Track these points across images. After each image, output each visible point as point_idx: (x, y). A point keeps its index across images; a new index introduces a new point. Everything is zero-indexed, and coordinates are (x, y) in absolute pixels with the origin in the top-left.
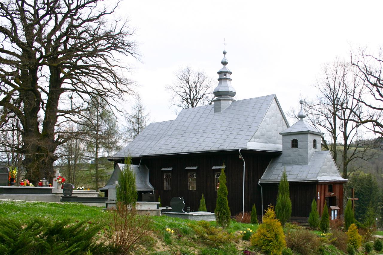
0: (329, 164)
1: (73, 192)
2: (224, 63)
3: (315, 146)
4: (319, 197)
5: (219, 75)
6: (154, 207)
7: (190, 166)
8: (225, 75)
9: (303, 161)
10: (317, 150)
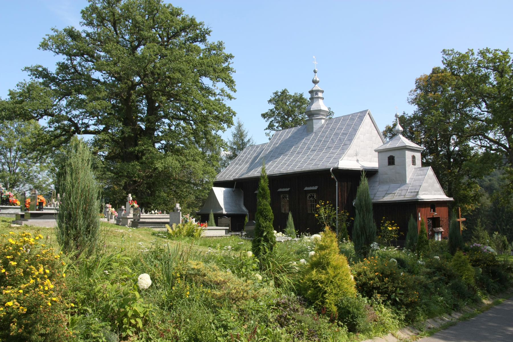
0: (430, 181)
1: (141, 217)
3: (414, 163)
4: (420, 219)
6: (223, 233)
7: (282, 188)
8: (317, 94)
9: (401, 180)
10: (416, 167)
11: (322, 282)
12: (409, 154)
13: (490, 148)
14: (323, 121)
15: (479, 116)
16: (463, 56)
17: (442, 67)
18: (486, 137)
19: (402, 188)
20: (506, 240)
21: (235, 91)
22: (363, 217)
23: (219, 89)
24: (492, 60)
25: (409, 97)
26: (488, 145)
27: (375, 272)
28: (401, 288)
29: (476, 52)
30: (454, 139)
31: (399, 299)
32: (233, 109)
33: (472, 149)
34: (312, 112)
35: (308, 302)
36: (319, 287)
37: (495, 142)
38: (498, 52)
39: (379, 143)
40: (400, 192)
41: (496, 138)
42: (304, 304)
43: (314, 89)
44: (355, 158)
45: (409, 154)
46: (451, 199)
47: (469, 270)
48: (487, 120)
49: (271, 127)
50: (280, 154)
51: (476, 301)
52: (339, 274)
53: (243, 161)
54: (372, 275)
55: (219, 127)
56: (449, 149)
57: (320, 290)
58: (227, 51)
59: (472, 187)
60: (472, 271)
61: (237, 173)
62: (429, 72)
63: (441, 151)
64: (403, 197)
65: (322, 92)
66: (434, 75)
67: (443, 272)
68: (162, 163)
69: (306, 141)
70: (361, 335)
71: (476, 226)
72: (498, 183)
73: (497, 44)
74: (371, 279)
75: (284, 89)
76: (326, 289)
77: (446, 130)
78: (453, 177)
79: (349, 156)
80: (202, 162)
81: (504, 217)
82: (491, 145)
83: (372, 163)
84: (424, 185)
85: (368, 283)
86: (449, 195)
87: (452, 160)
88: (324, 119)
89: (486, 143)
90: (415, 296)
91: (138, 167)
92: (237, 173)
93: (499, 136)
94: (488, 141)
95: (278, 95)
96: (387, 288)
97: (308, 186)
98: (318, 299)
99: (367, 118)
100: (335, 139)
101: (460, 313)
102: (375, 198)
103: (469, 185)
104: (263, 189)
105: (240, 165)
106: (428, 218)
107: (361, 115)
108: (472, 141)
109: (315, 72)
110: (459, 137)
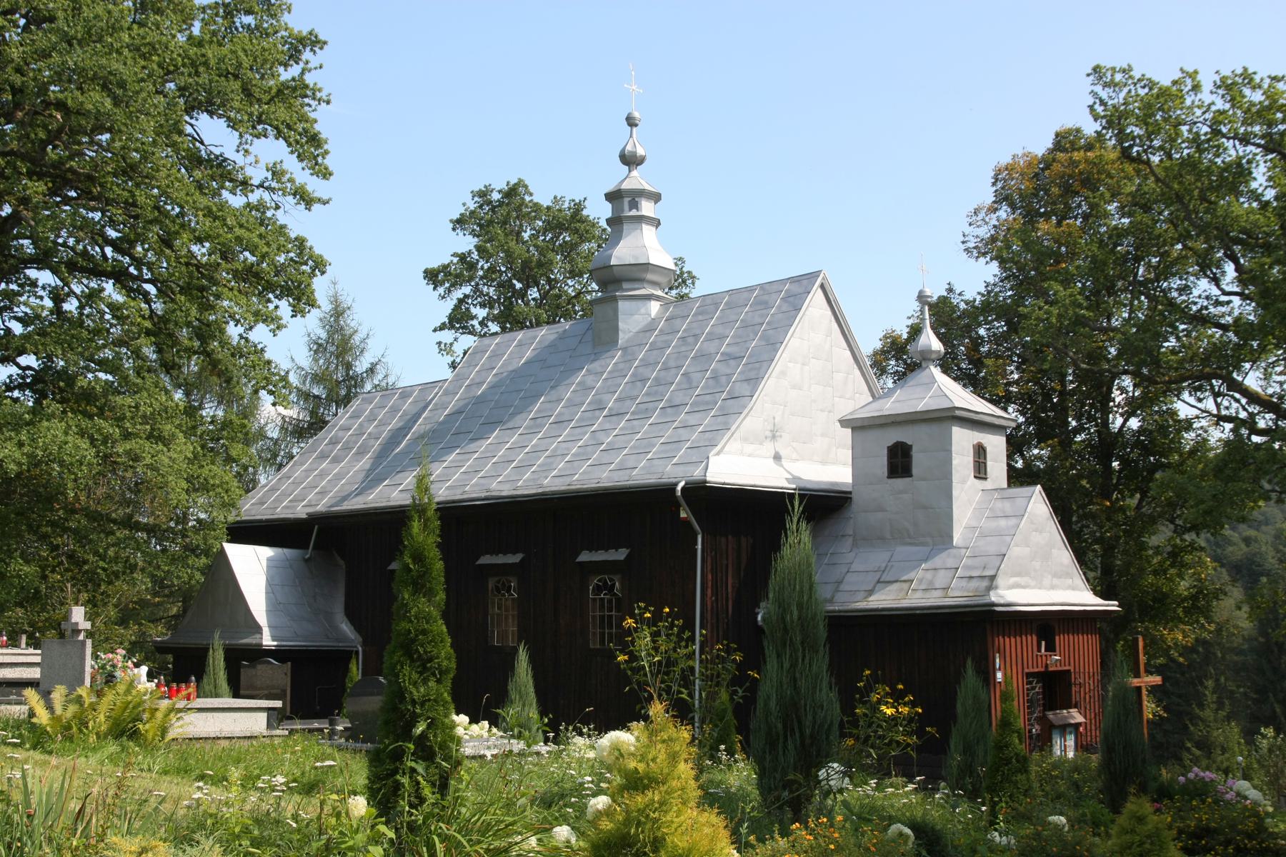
3: (980, 471)
4: (999, 675)
5: (610, 206)
8: (634, 205)
9: (933, 530)
12: (963, 439)
14: (655, 307)
15: (1212, 309)
17: (1091, 128)
19: (937, 561)
21: (326, 174)
22: (793, 666)
23: (262, 165)
25: (968, 230)
26: (1243, 415)
30: (1124, 388)
32: (318, 245)
33: (1188, 425)
40: (929, 575)
41: (1270, 391)
43: (625, 186)
44: (769, 449)
45: (963, 439)
46: (1113, 606)
50: (492, 424)
53: (347, 448)
56: (1106, 423)
58: (297, 21)
59: (1184, 565)
61: (323, 493)
62: (1041, 145)
64: (938, 593)
65: (656, 197)
68: (21, 445)
69: (590, 380)
75: (513, 181)
79: (745, 440)
82: (1252, 415)
83: (832, 467)
84: (1016, 552)
86: (1104, 591)
88: (658, 298)
89: (1235, 406)
92: (323, 493)
94: (1244, 401)
99: (815, 304)
100: (696, 376)
102: (840, 597)
103: (1175, 555)
104: (419, 558)
105: (336, 460)
106: (1029, 675)
107: (796, 288)
108: (1186, 395)
109: (631, 122)
110: (1140, 381)
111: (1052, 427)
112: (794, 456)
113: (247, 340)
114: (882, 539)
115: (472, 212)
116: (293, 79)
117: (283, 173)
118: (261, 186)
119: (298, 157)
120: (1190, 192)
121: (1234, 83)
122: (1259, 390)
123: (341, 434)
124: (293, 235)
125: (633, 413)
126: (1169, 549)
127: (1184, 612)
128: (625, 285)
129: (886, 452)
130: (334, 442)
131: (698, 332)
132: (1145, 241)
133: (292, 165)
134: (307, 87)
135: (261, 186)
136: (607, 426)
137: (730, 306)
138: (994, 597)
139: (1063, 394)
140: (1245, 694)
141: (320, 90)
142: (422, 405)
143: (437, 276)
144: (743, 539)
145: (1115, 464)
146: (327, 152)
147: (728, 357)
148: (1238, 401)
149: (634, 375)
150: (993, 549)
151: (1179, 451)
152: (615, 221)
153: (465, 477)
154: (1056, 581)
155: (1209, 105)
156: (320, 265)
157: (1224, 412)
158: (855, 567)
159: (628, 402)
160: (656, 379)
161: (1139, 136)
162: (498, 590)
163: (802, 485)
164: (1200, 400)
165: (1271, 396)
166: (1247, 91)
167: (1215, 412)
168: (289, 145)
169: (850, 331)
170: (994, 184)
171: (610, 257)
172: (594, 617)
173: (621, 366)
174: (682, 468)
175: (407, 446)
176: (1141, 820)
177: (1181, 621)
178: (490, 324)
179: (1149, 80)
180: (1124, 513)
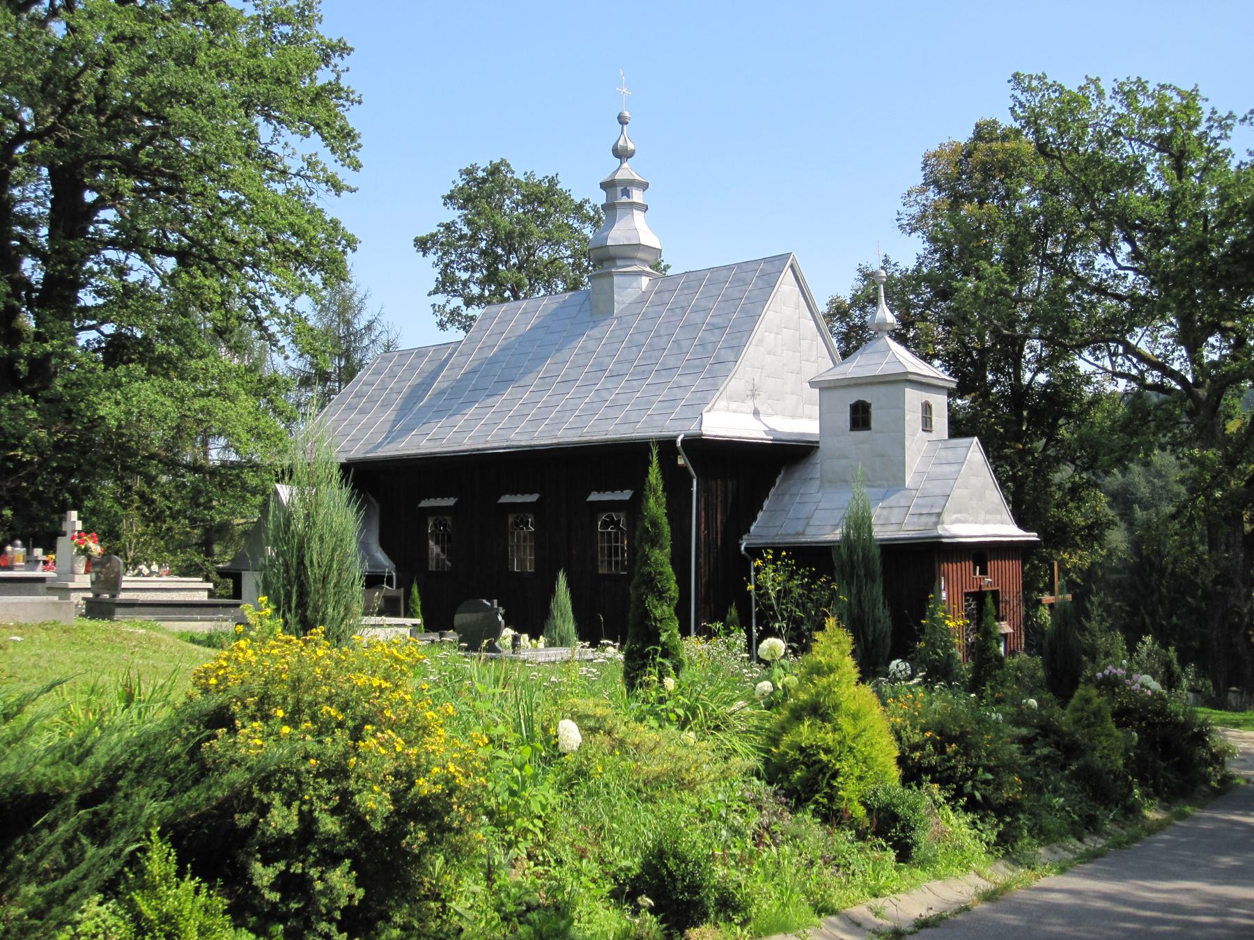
1: (124, 585)
2: (621, 154)
3: (927, 425)
4: (944, 594)
7: (514, 492)
8: (626, 193)
9: (890, 475)
11: (828, 751)
12: (913, 398)
13: (1139, 380)
14: (645, 282)
15: (1110, 282)
16: (1074, 99)
17: (1007, 122)
18: (1130, 350)
19: (892, 501)
20: (1175, 661)
21: (357, 167)
22: (859, 592)
23: (298, 156)
24: (1154, 117)
25: (902, 209)
26: (1134, 372)
27: (924, 731)
28: (988, 769)
29: (1107, 86)
30: (1033, 348)
31: (983, 796)
32: (349, 226)
33: (1087, 380)
34: (612, 252)
35: (797, 798)
36: (820, 761)
37: (1154, 365)
38: (1168, 93)
39: (818, 357)
40: (885, 513)
41: (1157, 352)
42: (786, 804)
43: (618, 176)
44: (749, 406)
45: (913, 398)
46: (1033, 537)
47: (1109, 735)
48: (1132, 297)
49: (446, 283)
50: (506, 381)
51: (1132, 811)
52: (864, 730)
53: (372, 401)
54: (917, 738)
55: (301, 287)
56: (1018, 378)
57: (824, 768)
58: (327, 31)
59: (1081, 499)
60: (1117, 738)
61: (354, 440)
62: (964, 136)
63: (993, 384)
64: (894, 527)
65: (644, 186)
66: (981, 145)
67: (1053, 737)
68: (117, 403)
69: (591, 345)
70: (918, 872)
71: (1088, 618)
72: (1149, 482)
73: (1166, 67)
74: (915, 747)
75: (497, 161)
76: (838, 766)
77: (1012, 322)
78: (1028, 465)
79: (731, 399)
80: (246, 403)
81: (1164, 590)
82: (1141, 372)
83: (801, 422)
84: (957, 493)
85: (908, 757)
86: (1021, 522)
87: (1025, 413)
88: (647, 274)
89: (1126, 365)
90: (1012, 790)
91: (32, 415)
92: (354, 440)
93: (1165, 346)
94: (1135, 360)
95: (475, 179)
96: (954, 768)
97: (600, 489)
98: (817, 792)
99: (786, 284)
100: (685, 343)
101: (1101, 837)
102: (810, 531)
103: (1074, 491)
104: (655, 524)
105: (363, 412)
106: (967, 594)
107: (768, 268)
108: (1086, 354)
109: (622, 120)
110: (1048, 341)
111: (973, 381)
112: (770, 411)
113: (293, 310)
114: (845, 481)
115: (462, 188)
116: (330, 83)
117: (317, 163)
118: (298, 174)
119: (332, 149)
120: (1095, 184)
121: (1130, 91)
122: (1148, 351)
123: (365, 388)
124: (328, 218)
125: (632, 374)
126: (1069, 485)
127: (1082, 539)
128: (619, 263)
129: (848, 409)
130: (359, 396)
131: (685, 304)
132: (1053, 220)
133: (327, 158)
134: (341, 89)
135: (298, 174)
136: (609, 385)
137: (711, 282)
138: (940, 531)
139: (982, 352)
140: (1120, 607)
141: (353, 92)
142: (437, 363)
143: (425, 244)
144: (730, 484)
145: (1025, 413)
146: (360, 146)
147: (713, 327)
148: (1130, 360)
149: (630, 341)
150: (938, 491)
151: (1079, 401)
152: (610, 207)
153: (485, 428)
154: (988, 517)
155: (1110, 109)
156: (351, 243)
157: (1118, 370)
158: (821, 505)
159: (626, 365)
160: (650, 344)
161: (1052, 135)
162: (517, 525)
163: (778, 437)
164: (1097, 359)
165: (1158, 357)
166: (1140, 98)
167: (1110, 368)
168: (324, 139)
169: (814, 304)
170: (923, 169)
171: (606, 238)
172: (602, 548)
173: (618, 333)
174: (679, 423)
175: (430, 400)
176: (1088, 701)
177: (1077, 546)
178: (471, 285)
179: (1060, 86)
180: (1033, 455)
